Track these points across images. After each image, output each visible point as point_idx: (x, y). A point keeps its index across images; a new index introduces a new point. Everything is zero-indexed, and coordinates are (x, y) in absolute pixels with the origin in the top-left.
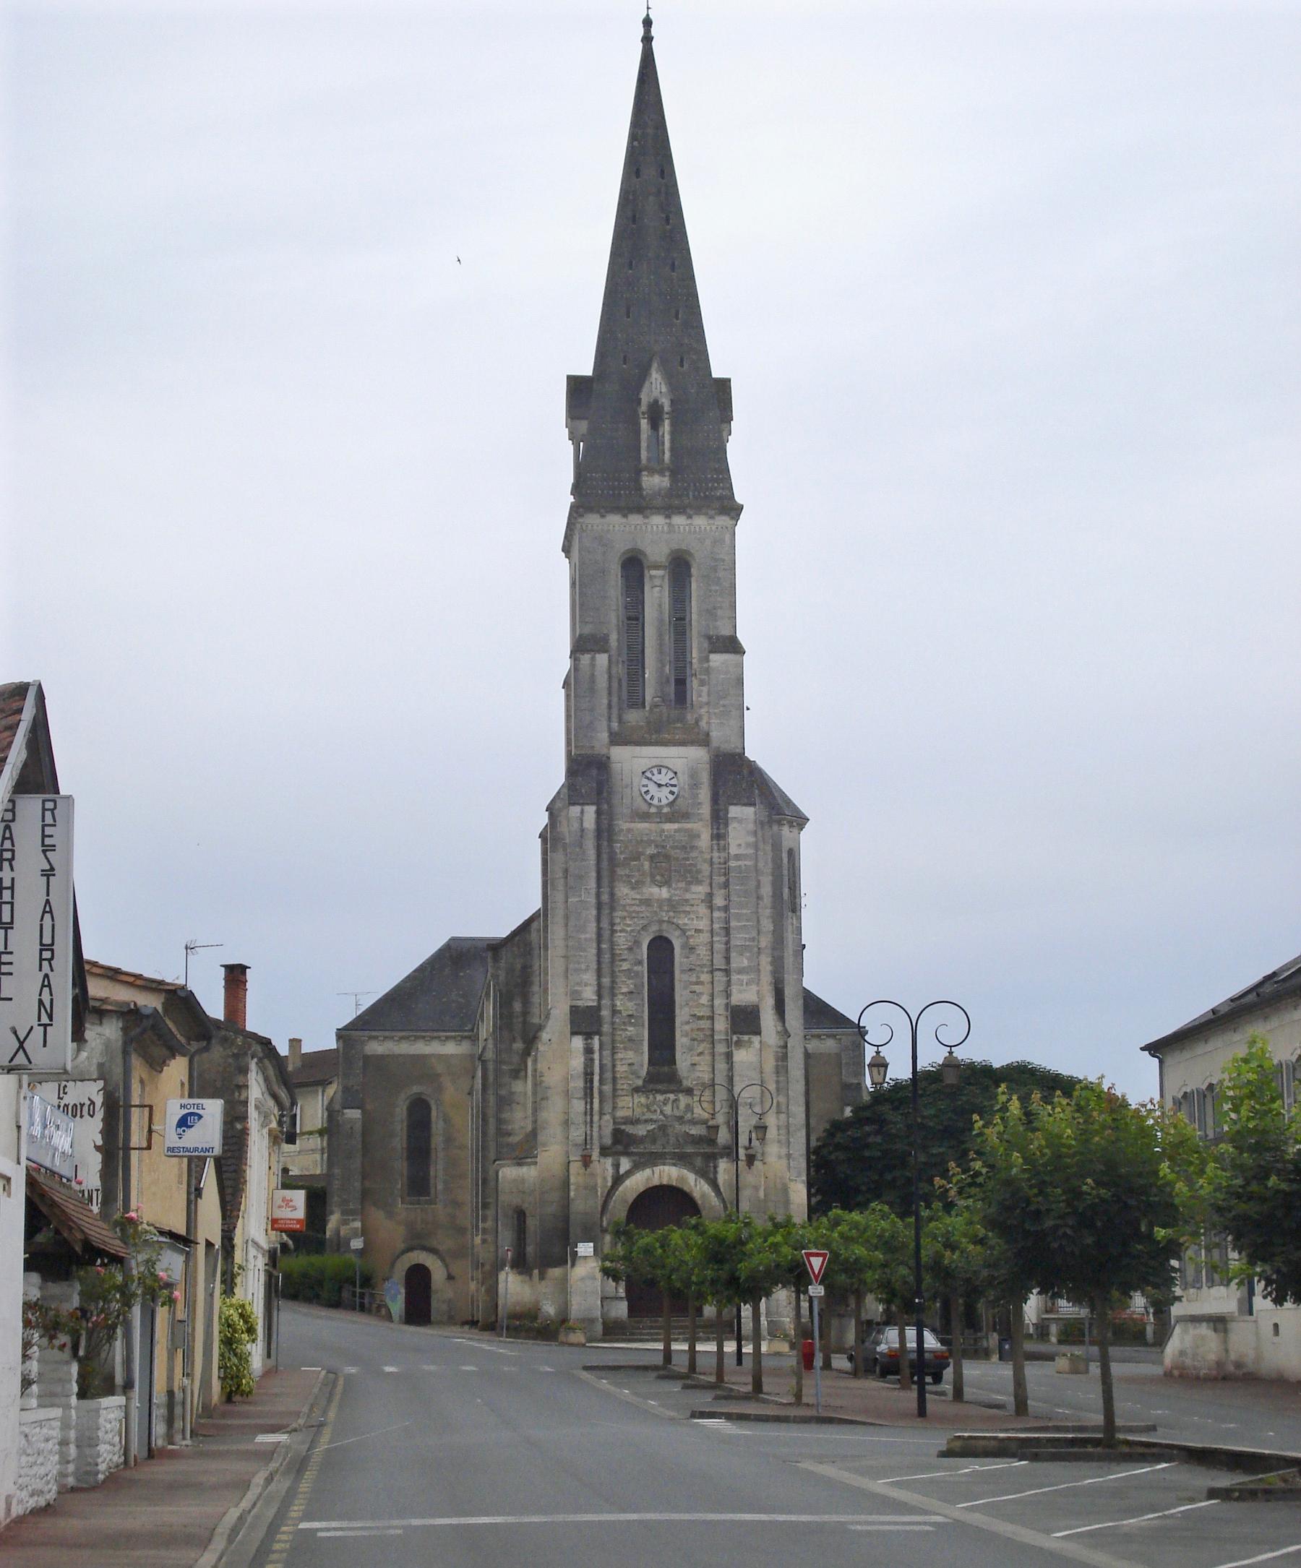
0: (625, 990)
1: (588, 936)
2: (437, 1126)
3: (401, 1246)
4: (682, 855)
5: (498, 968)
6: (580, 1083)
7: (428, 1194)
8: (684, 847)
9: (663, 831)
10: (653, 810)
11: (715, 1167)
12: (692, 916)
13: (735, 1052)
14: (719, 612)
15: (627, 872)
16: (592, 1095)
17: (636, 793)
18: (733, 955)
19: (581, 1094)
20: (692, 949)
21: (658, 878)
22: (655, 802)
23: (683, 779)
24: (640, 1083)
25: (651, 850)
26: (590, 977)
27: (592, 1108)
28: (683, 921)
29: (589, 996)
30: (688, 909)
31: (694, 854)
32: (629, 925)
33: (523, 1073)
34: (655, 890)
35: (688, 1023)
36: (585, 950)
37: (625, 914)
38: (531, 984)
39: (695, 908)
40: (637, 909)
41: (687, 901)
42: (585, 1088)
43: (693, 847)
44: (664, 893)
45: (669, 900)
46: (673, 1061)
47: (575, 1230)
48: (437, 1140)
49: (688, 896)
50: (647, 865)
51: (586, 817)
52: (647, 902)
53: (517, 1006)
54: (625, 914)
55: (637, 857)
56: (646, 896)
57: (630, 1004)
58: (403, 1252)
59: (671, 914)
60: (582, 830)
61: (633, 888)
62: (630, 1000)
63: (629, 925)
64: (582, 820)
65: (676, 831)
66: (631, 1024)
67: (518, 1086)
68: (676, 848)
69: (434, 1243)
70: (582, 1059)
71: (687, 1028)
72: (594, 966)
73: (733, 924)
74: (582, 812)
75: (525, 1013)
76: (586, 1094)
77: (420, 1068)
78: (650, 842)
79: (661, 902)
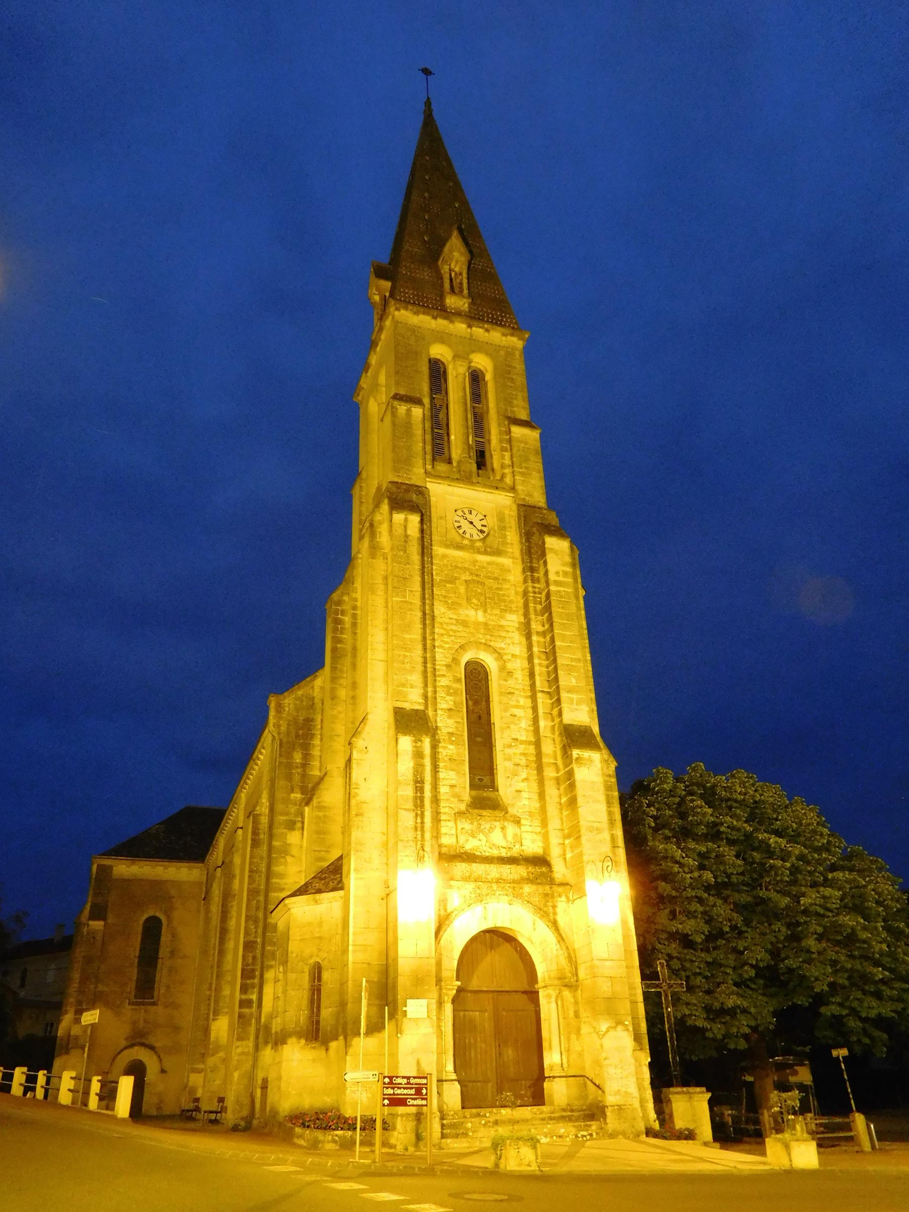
0: (444, 706)
1: (413, 636)
2: (165, 938)
3: (124, 1043)
4: (496, 586)
5: (280, 718)
6: (408, 792)
7: (152, 997)
8: (496, 579)
9: (476, 561)
10: (466, 542)
11: (554, 907)
12: (508, 641)
13: (576, 770)
14: (515, 402)
15: (443, 592)
16: (422, 806)
17: (450, 526)
18: (561, 673)
19: (410, 805)
20: (510, 673)
21: (475, 601)
22: (468, 536)
23: (492, 522)
24: (463, 807)
25: (466, 577)
26: (416, 678)
27: (422, 823)
28: (498, 645)
29: (414, 700)
30: (503, 634)
31: (505, 586)
32: (447, 643)
33: (299, 825)
34: (472, 613)
35: (510, 746)
36: (410, 650)
37: (443, 632)
38: (312, 736)
39: (510, 635)
40: (454, 628)
41: (501, 626)
42: (415, 798)
43: (504, 580)
44: (480, 616)
45: (486, 624)
46: (493, 786)
47: (403, 982)
48: (163, 952)
49: (503, 623)
50: (462, 589)
51: (410, 526)
52: (464, 623)
53: (298, 757)
54: (443, 632)
55: (453, 581)
56: (462, 617)
57: (450, 722)
58: (126, 1048)
59: (488, 637)
60: (407, 536)
61: (449, 608)
62: (450, 717)
63: (447, 643)
64: (405, 527)
65: (489, 563)
66: (452, 743)
67: (293, 838)
68: (489, 578)
69: (151, 1040)
70: (411, 764)
71: (508, 751)
72: (420, 668)
73: (558, 643)
74: (406, 520)
75: (305, 765)
76: (416, 806)
77: (158, 891)
78: (465, 569)
79: (477, 624)
